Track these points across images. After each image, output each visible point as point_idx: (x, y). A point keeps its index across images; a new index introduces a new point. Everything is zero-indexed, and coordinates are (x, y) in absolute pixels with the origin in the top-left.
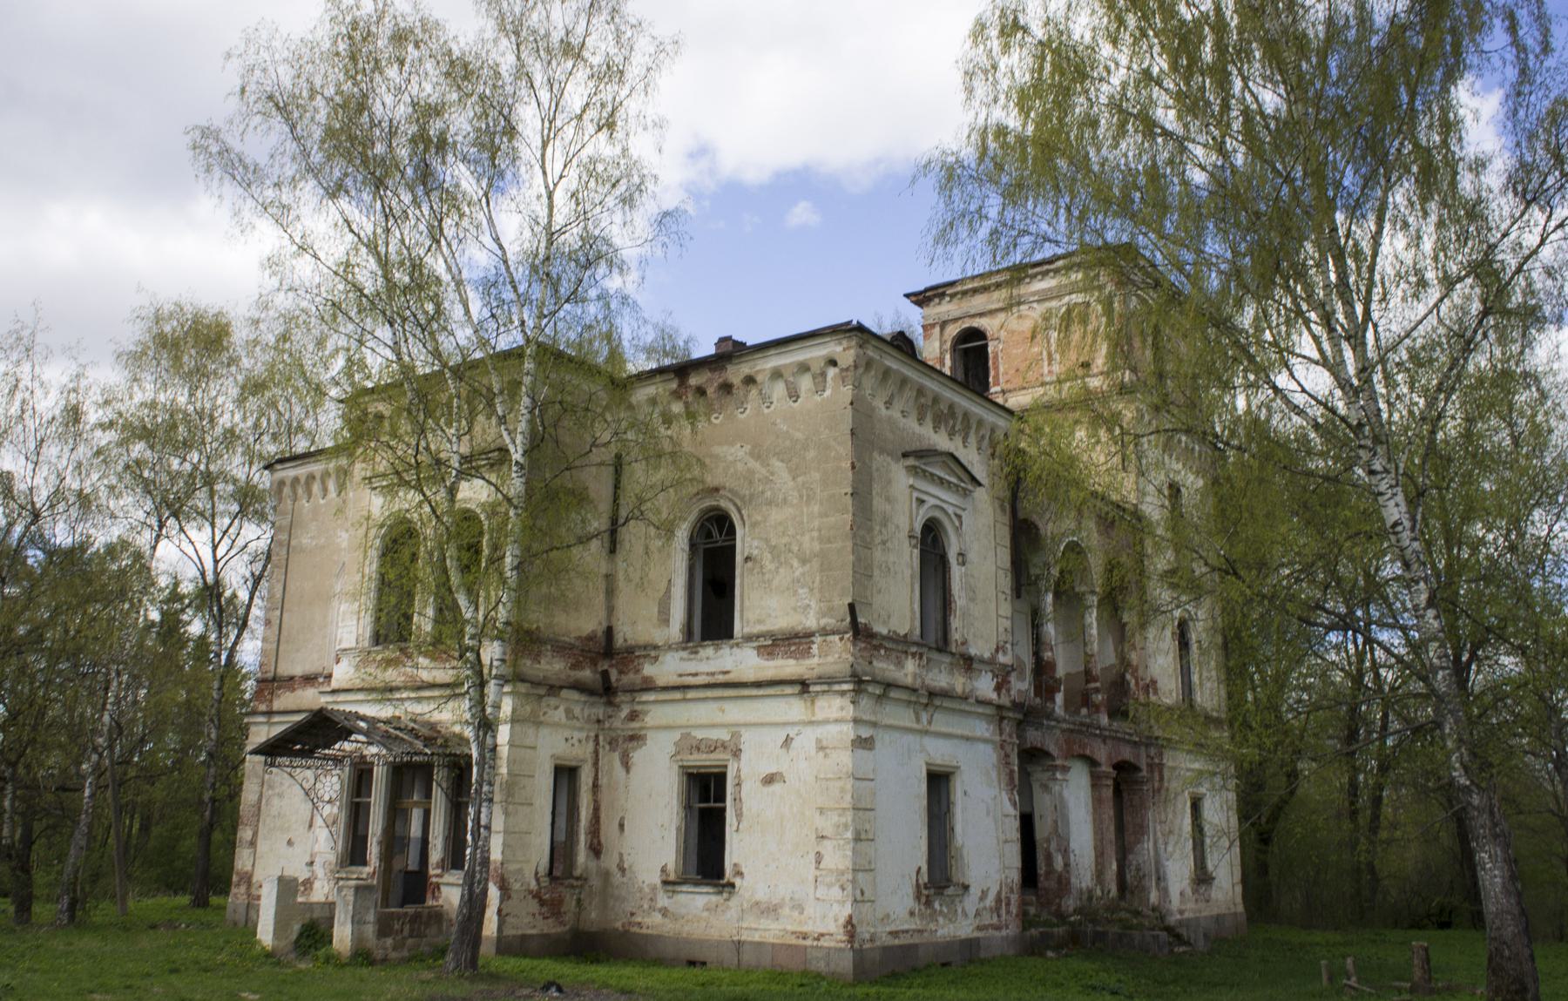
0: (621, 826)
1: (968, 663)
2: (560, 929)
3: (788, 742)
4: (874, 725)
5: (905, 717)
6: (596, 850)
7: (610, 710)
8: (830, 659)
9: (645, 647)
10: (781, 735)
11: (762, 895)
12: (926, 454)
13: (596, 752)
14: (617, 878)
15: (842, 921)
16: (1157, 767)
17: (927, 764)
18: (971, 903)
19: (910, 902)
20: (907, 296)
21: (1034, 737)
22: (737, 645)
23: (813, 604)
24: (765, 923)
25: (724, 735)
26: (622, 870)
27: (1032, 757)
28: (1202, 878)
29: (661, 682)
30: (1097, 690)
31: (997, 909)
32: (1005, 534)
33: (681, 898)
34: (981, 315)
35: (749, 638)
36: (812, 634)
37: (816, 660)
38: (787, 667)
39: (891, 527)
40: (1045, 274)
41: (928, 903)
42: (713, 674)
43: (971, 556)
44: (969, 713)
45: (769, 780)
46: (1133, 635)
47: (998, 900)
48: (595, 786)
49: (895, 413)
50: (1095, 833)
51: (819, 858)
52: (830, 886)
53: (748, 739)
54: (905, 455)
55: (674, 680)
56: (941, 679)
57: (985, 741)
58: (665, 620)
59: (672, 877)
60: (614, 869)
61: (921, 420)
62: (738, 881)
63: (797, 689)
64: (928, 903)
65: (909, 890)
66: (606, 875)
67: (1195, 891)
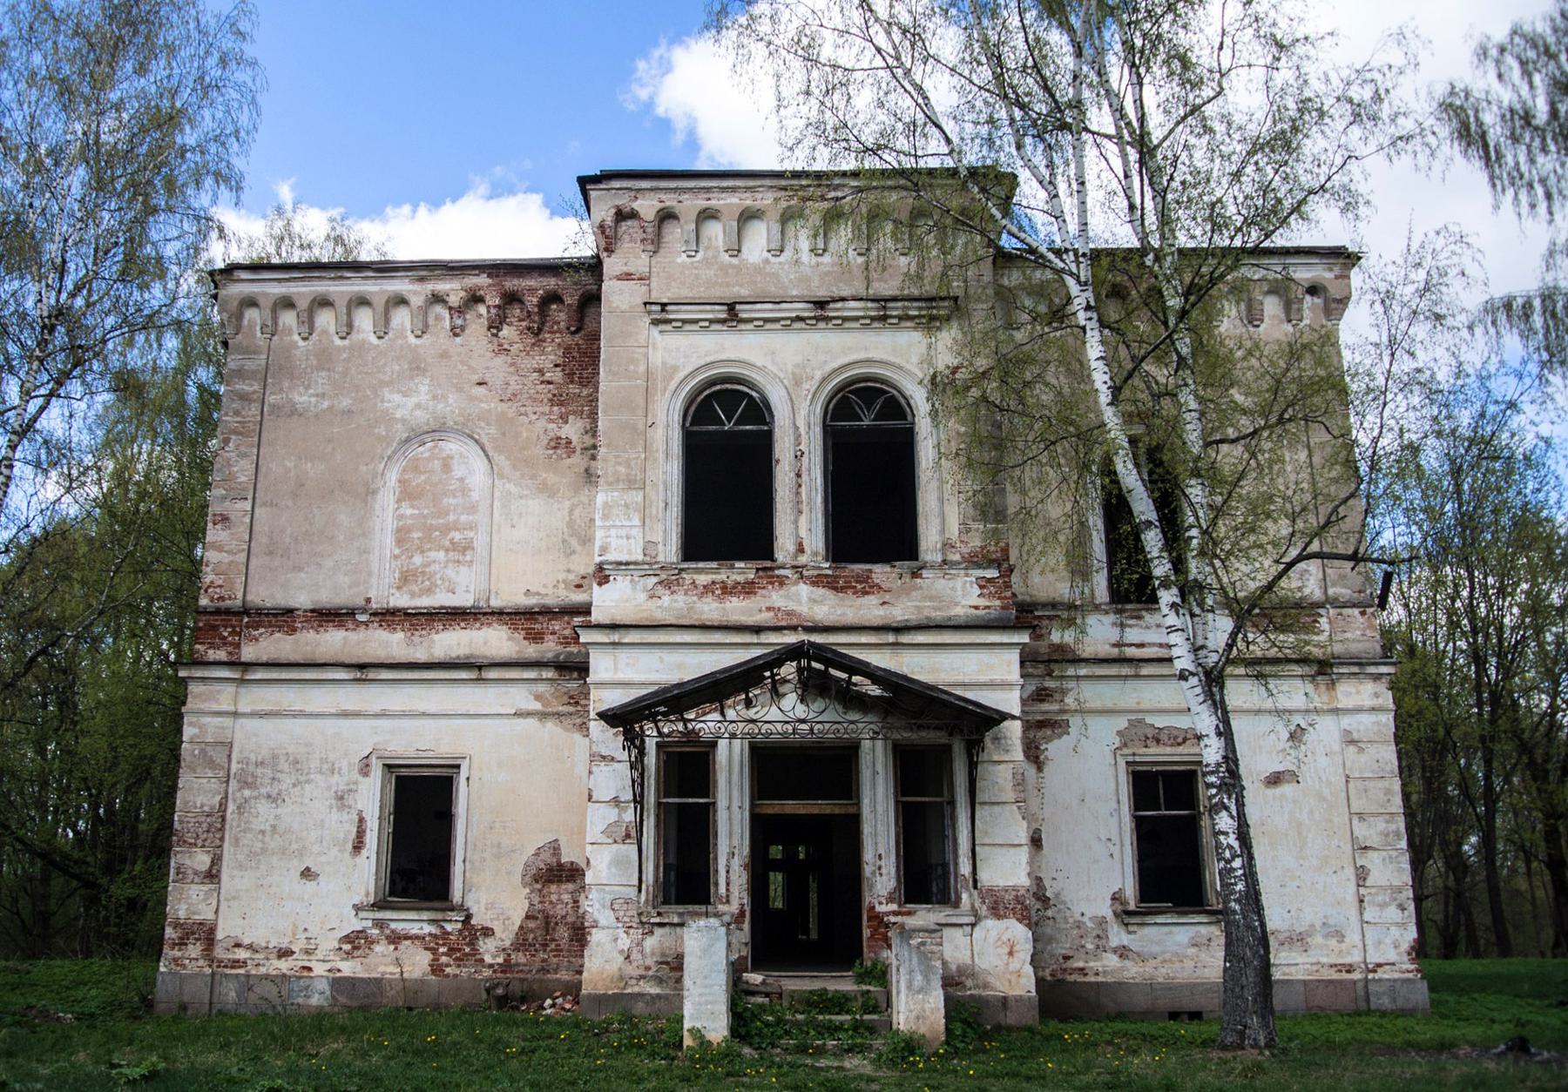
45: (1275, 780)
51: (1362, 875)
52: (1383, 905)
59: (1132, 906)
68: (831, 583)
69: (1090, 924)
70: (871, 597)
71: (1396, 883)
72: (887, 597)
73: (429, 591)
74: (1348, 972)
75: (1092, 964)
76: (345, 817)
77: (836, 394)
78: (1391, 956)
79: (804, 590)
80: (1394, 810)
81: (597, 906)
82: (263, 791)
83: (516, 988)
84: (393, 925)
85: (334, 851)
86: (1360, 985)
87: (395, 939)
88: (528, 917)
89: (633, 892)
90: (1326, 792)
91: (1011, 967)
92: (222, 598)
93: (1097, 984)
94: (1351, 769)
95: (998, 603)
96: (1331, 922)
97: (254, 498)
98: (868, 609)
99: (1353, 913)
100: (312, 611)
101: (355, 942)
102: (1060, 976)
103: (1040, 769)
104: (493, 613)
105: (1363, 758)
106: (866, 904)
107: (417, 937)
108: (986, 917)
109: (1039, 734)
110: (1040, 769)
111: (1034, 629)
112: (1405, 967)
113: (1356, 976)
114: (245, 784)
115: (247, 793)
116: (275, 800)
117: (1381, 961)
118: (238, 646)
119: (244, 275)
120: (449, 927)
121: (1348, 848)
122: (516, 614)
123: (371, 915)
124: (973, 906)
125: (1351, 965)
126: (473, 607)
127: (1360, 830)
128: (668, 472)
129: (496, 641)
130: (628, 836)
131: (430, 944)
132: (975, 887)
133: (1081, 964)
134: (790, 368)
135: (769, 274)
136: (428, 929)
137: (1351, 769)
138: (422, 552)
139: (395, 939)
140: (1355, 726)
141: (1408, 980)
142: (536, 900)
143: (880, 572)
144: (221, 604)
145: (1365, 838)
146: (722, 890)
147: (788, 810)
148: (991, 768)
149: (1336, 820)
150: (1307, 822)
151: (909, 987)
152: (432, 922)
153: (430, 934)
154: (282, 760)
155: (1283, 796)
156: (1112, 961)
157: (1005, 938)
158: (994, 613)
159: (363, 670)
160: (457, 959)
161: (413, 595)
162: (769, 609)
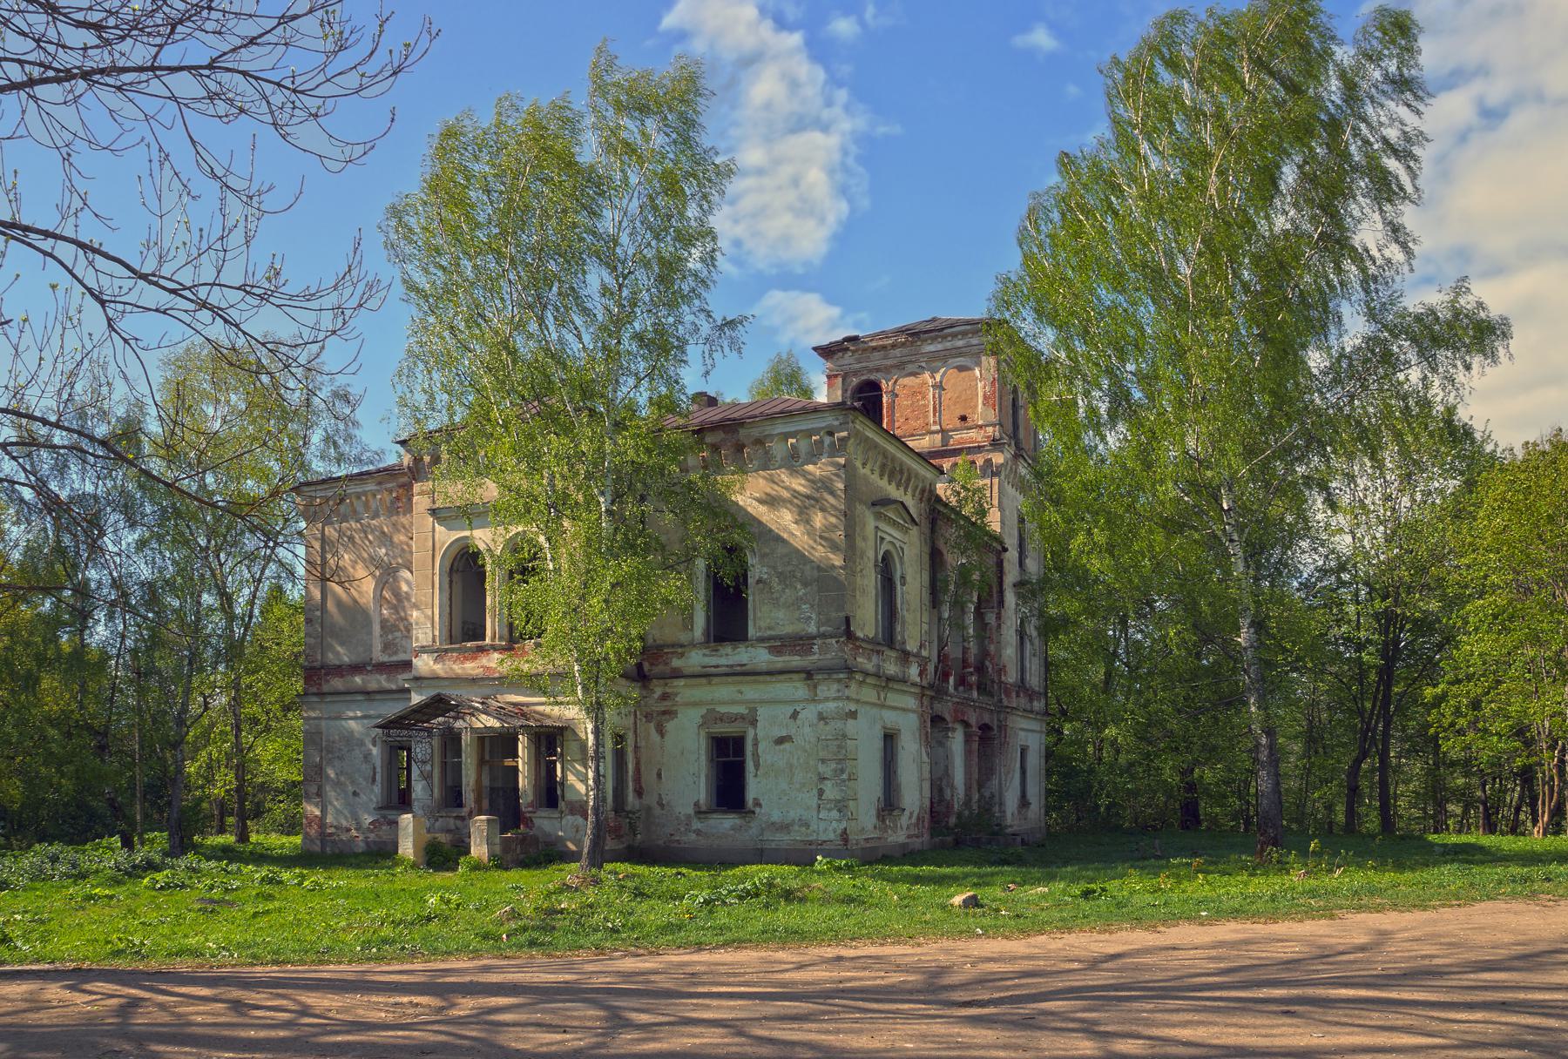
0: (659, 775)
1: (905, 656)
2: (621, 846)
3: (795, 715)
4: (858, 701)
5: (869, 694)
6: (639, 793)
7: (644, 693)
8: (829, 656)
9: (673, 646)
10: (789, 710)
11: (776, 816)
12: (886, 502)
13: (635, 723)
14: (657, 811)
15: (839, 831)
16: (1002, 728)
17: (885, 728)
18: (904, 820)
19: (874, 820)
20: (815, 349)
21: (938, 707)
22: (752, 646)
23: (814, 616)
24: (778, 836)
25: (742, 710)
26: (662, 805)
27: (937, 720)
28: (1024, 802)
29: (687, 671)
30: (972, 674)
31: (917, 825)
32: (926, 558)
33: (712, 822)
34: (878, 370)
35: (762, 640)
36: (814, 638)
37: (816, 657)
38: (795, 661)
39: (865, 559)
40: (934, 339)
41: (883, 821)
42: (732, 666)
43: (908, 579)
44: (904, 692)
45: (781, 741)
46: (142, 505)
47: (918, 819)
48: (636, 747)
49: (867, 471)
50: (966, 773)
51: (821, 792)
52: (830, 810)
53: (762, 713)
54: (874, 504)
55: (698, 670)
56: (892, 669)
57: (914, 711)
58: (688, 623)
59: (704, 808)
60: (654, 804)
61: (881, 476)
62: (757, 810)
63: (804, 675)
64: (883, 821)
65: (873, 812)
66: (649, 809)
67: (1019, 812)
73: (395, 653)
78: (832, 836)
79: (496, 655)
83: (506, 631)
90: (807, 747)
98: (471, 668)
99: (815, 814)
103: (662, 736)
110: (662, 736)
111: (39, 666)
114: (329, 752)
127: (821, 768)
156: (693, 836)
161: (390, 655)
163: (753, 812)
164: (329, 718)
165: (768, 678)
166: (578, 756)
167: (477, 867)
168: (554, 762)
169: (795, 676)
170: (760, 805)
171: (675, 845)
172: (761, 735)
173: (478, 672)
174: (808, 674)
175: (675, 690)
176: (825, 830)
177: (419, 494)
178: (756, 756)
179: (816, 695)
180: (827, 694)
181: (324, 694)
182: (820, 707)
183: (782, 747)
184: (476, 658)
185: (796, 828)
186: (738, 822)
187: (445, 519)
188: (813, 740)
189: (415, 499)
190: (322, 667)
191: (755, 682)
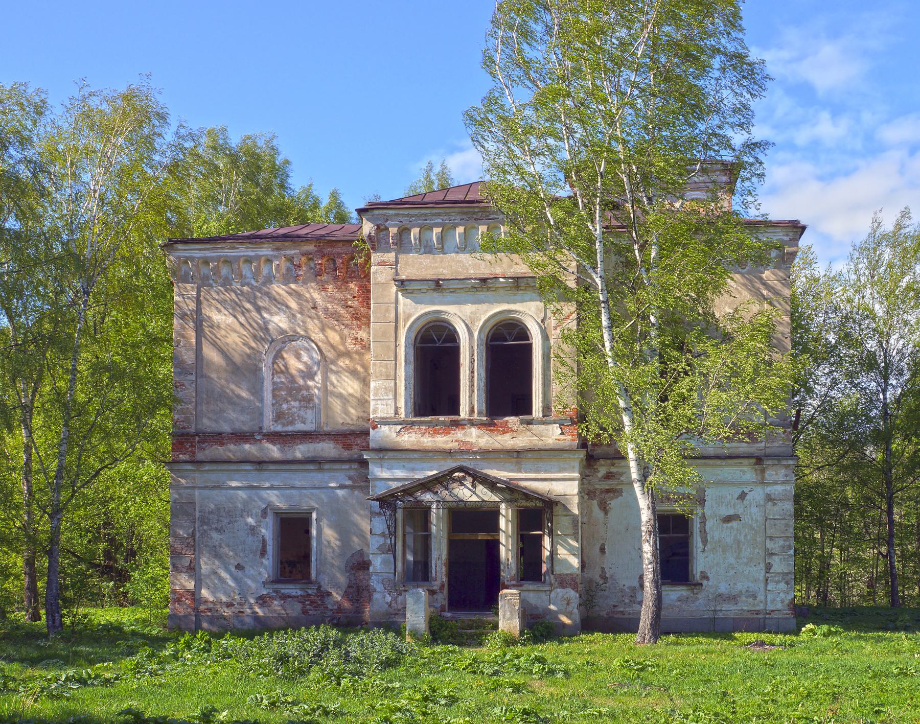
0: (602, 550)
3: (742, 496)
8: (776, 444)
10: (737, 491)
11: (723, 588)
15: (787, 602)
24: (725, 607)
45: (728, 519)
51: (768, 567)
52: (778, 582)
53: (710, 493)
62: (705, 582)
63: (753, 461)
68: (488, 426)
69: (627, 590)
70: (508, 435)
71: (785, 571)
72: (515, 435)
73: (292, 423)
74: (757, 614)
75: (627, 609)
76: (256, 539)
77: (493, 327)
78: (779, 606)
79: (474, 431)
80: (789, 535)
81: (375, 582)
82: (214, 526)
84: (283, 591)
85: (251, 556)
86: (762, 621)
87: (284, 597)
88: (349, 587)
89: (392, 576)
90: (754, 525)
91: (568, 610)
92: (184, 428)
93: (630, 619)
94: (768, 514)
95: (570, 437)
96: (751, 589)
97: (196, 373)
99: (762, 585)
100: (232, 434)
101: (262, 601)
102: (611, 615)
103: (606, 514)
104: (325, 435)
105: (776, 508)
106: (501, 581)
107: (295, 597)
108: (557, 588)
109: (607, 496)
110: (606, 514)
112: (785, 612)
113: (761, 616)
115: (205, 527)
116: (220, 531)
117: (774, 609)
118: (194, 452)
119: (180, 246)
120: (310, 592)
121: (762, 554)
122: (337, 435)
123: (271, 586)
124: (551, 582)
125: (758, 611)
126: (315, 431)
127: (770, 545)
128: (403, 372)
129: (328, 449)
130: (389, 550)
131: (301, 600)
132: (553, 574)
133: (622, 609)
134: (468, 314)
135: (458, 261)
136: (300, 593)
137: (768, 514)
138: (287, 402)
139: (284, 597)
140: (773, 491)
141: (786, 618)
142: (353, 578)
143: (512, 420)
144: (184, 431)
145: (772, 548)
146: (434, 575)
147: (466, 538)
148: (557, 518)
149: (758, 540)
150: (743, 540)
151: (504, 618)
152: (301, 589)
153: (301, 595)
154: (222, 510)
155: (732, 528)
157: (565, 597)
158: (567, 443)
159: (261, 464)
160: (315, 607)
161: (284, 425)
162: (456, 441)
163: (701, 584)
164: (205, 488)
165: (718, 462)
166: (570, 531)
167: (509, 642)
168: (540, 538)
169: (745, 461)
170: (707, 578)
171: (621, 616)
172: (708, 512)
173: (454, 446)
174: (759, 460)
175: (620, 470)
176: (773, 601)
177: (379, 264)
178: (703, 532)
179: (763, 478)
180: (775, 478)
181: (201, 462)
182: (768, 490)
183: (729, 525)
184: (448, 432)
185: (744, 598)
186: (685, 593)
187: (413, 292)
188: (761, 519)
189: (373, 269)
190: (197, 435)
191: (706, 465)
